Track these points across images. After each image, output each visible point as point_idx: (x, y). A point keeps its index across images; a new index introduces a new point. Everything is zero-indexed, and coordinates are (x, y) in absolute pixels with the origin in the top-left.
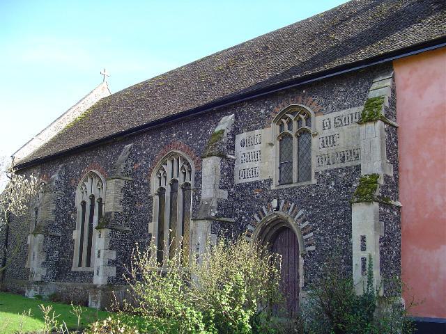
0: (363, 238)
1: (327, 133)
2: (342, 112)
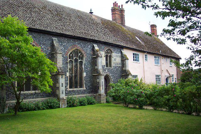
1: (115, 58)
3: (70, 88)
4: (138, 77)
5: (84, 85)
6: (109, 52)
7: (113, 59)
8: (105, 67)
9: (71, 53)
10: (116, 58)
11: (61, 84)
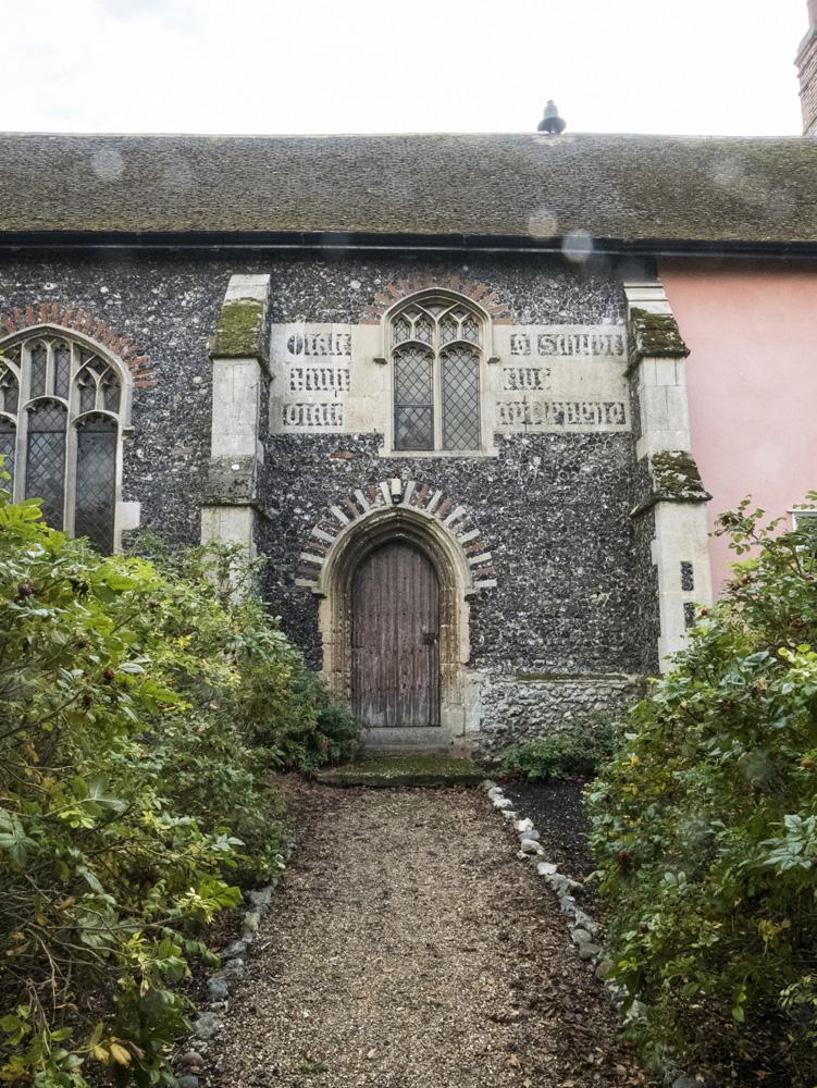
0: (687, 569)
2: (556, 329)
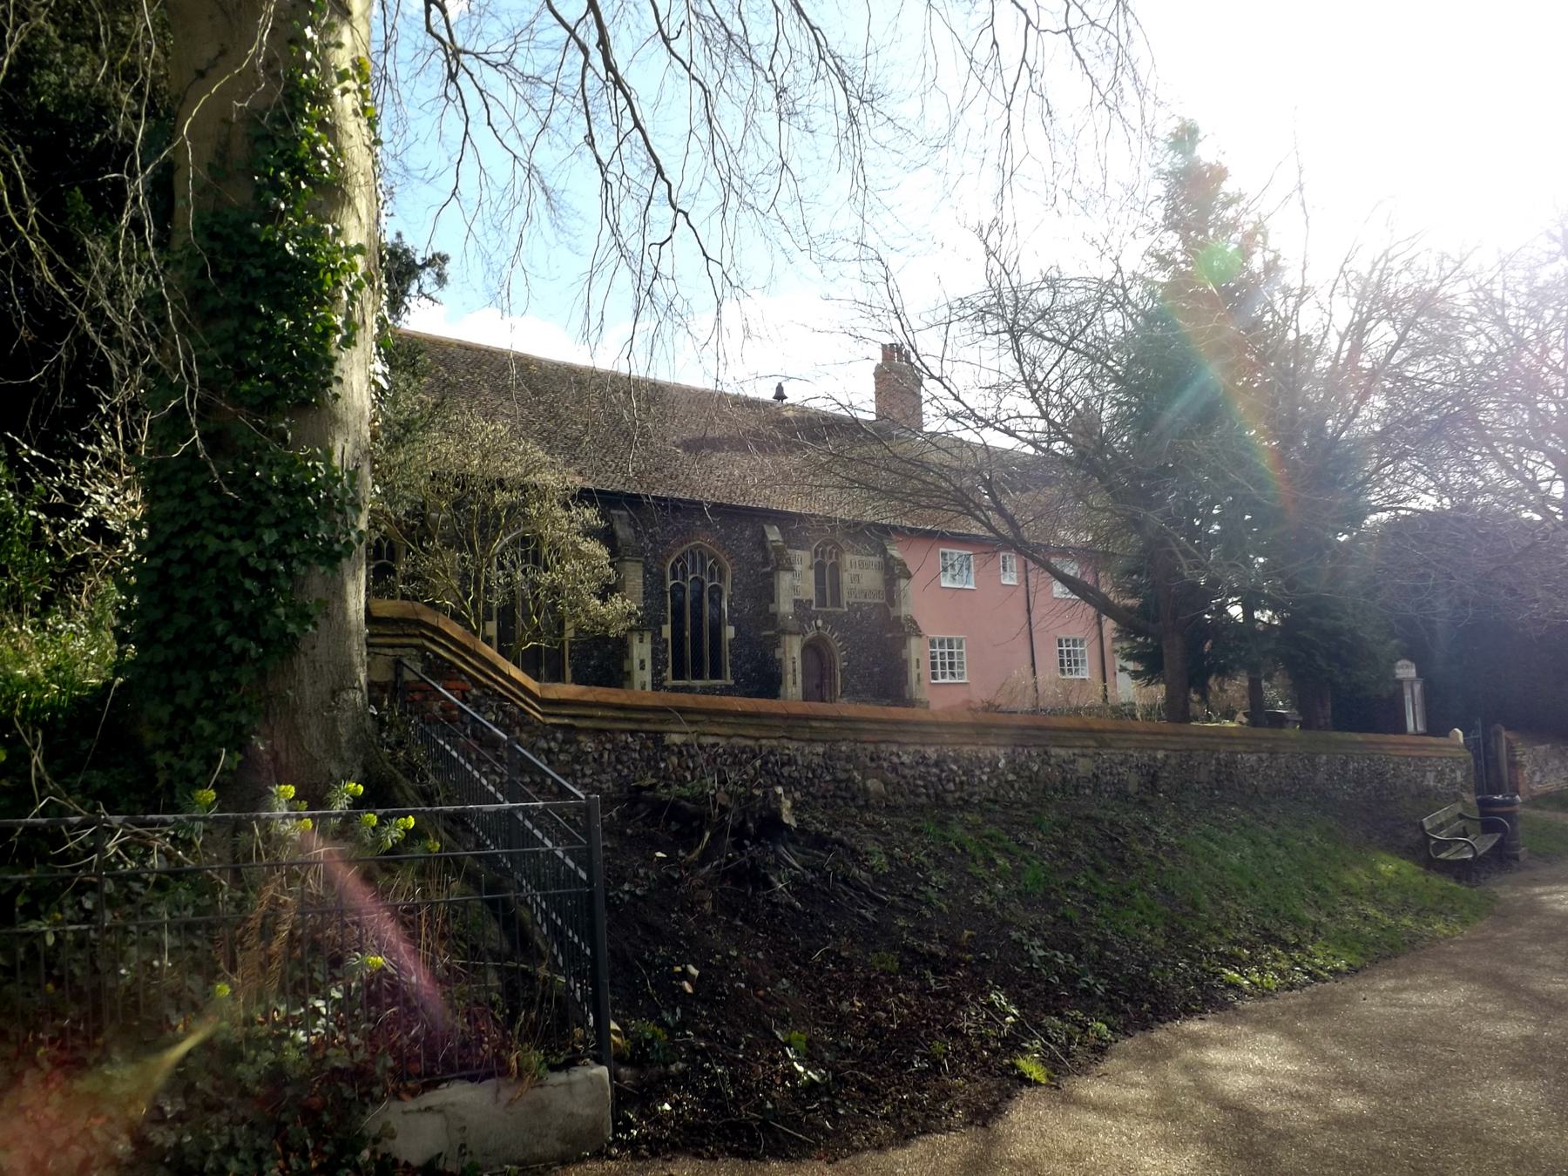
1: (853, 571)
3: (674, 678)
4: (1070, 270)
5: (729, 669)
6: (831, 552)
7: (846, 577)
8: (813, 608)
9: (678, 560)
10: (858, 571)
11: (636, 663)
